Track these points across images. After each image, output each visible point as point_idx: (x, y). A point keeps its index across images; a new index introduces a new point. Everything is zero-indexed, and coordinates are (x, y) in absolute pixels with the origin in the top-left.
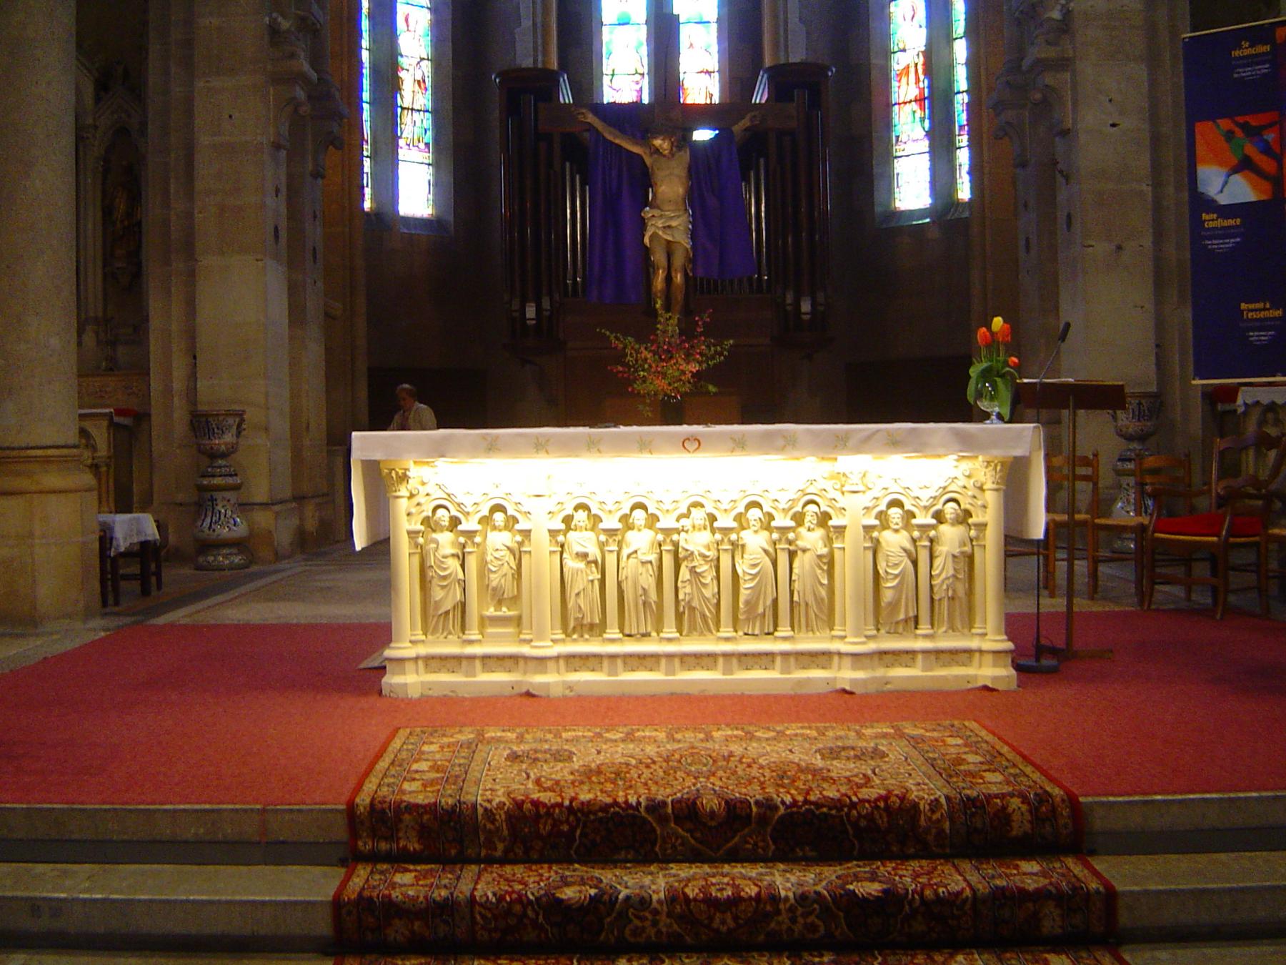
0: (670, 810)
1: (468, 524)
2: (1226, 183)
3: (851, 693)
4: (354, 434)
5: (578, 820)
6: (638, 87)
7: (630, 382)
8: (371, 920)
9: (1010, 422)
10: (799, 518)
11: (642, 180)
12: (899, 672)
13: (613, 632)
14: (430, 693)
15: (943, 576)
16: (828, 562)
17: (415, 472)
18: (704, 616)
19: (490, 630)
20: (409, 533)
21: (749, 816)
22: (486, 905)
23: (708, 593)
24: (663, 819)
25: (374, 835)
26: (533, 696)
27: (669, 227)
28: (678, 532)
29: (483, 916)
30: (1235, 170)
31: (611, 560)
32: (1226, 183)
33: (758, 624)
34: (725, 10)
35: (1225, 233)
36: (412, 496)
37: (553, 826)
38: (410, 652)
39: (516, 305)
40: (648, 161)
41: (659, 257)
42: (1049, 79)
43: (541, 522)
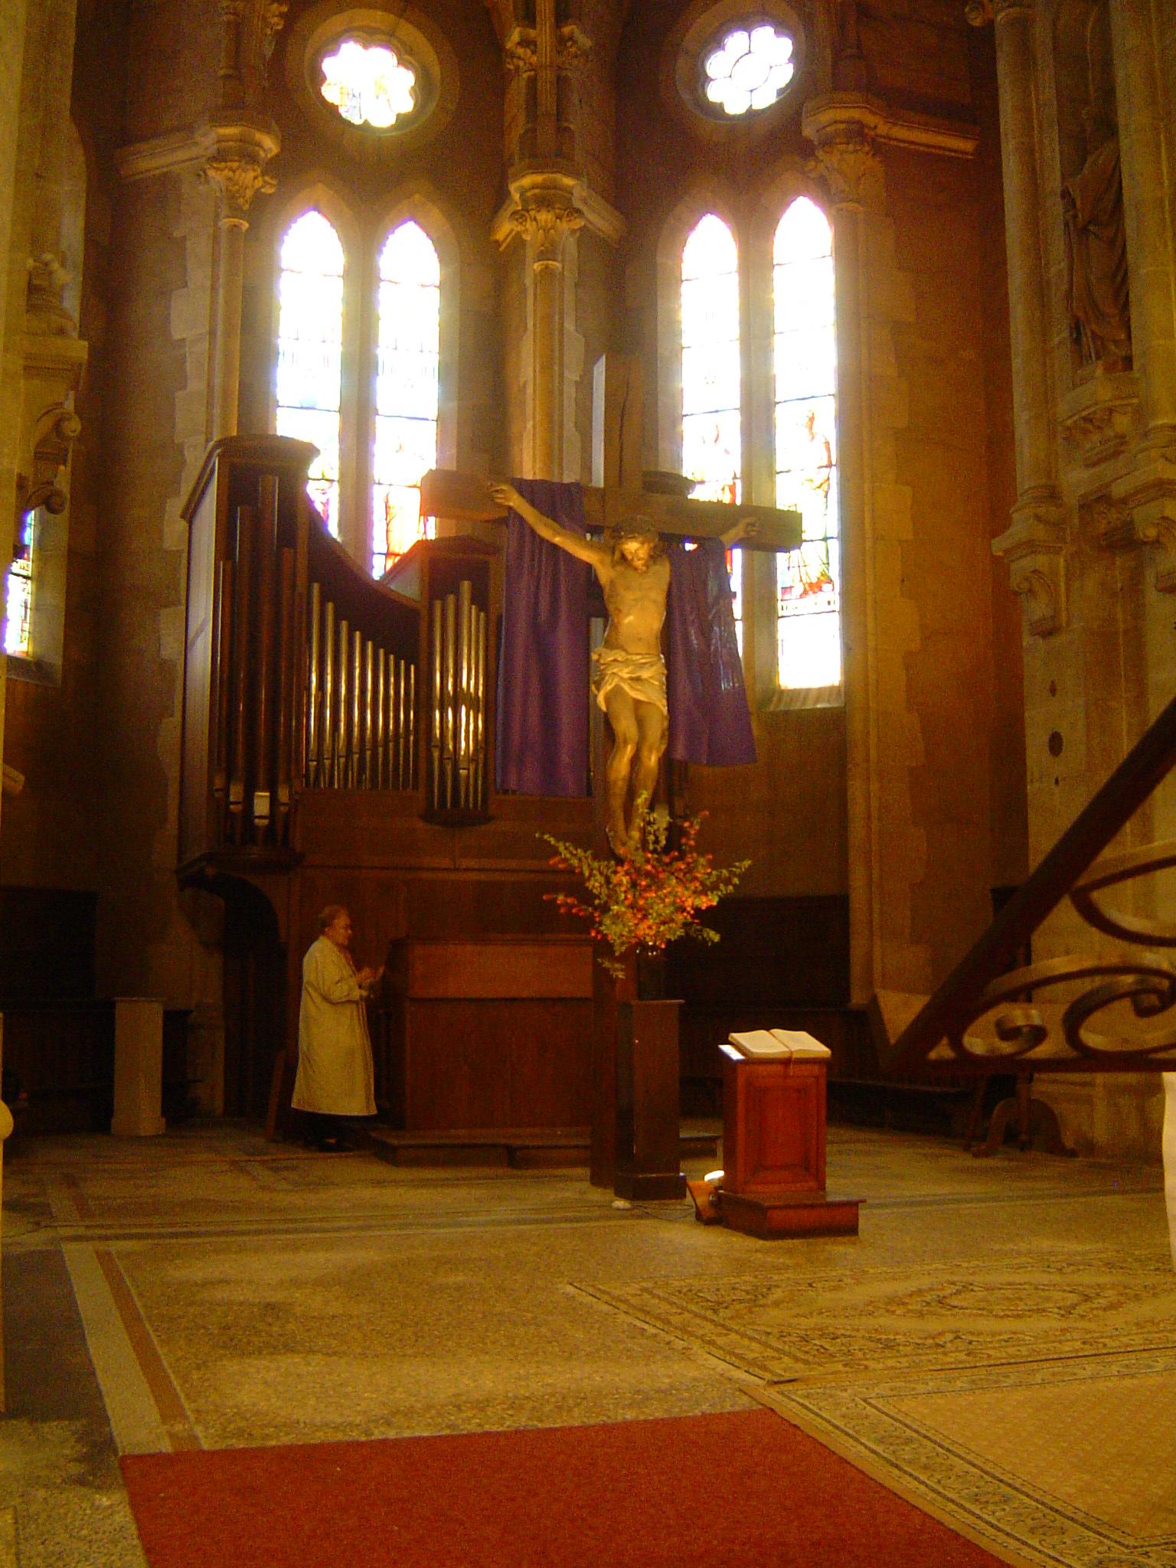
4: (294, 1105)
7: (589, 923)
11: (593, 602)
27: (638, 679)
34: (453, 405)
39: (236, 792)
40: (605, 574)
41: (625, 726)
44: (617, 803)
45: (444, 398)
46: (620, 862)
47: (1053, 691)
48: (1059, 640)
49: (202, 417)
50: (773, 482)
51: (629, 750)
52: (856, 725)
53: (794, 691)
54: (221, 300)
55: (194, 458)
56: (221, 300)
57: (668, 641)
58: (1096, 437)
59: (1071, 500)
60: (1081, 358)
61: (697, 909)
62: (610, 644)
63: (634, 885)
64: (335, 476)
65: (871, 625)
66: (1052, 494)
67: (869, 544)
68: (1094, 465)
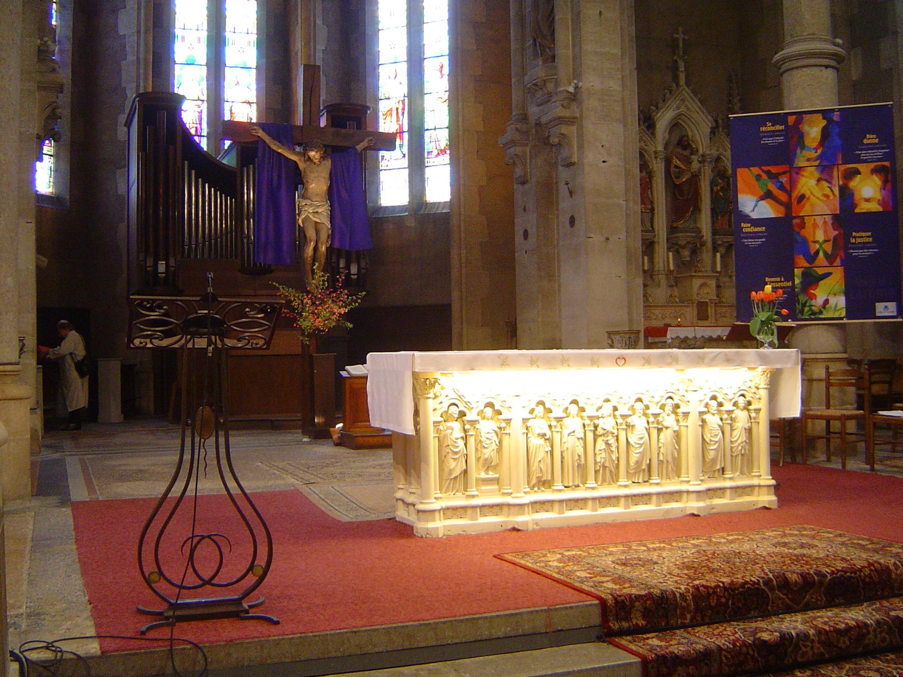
0: (775, 582)
1: (470, 416)
2: (756, 206)
3: (699, 516)
5: (730, 594)
6: (199, 110)
7: (295, 320)
8: (665, 669)
9: (778, 348)
10: (663, 407)
11: (297, 179)
12: (717, 501)
13: (558, 485)
14: (449, 533)
15: (740, 441)
16: (677, 435)
17: (443, 380)
18: (611, 471)
19: (483, 488)
20: (434, 422)
21: (814, 581)
22: (728, 651)
23: (614, 457)
24: (772, 589)
25: (618, 618)
26: (518, 530)
27: (317, 212)
28: (598, 418)
29: (726, 657)
30: (762, 198)
31: (557, 437)
32: (756, 206)
33: (641, 477)
35: (755, 235)
36: (436, 396)
37: (718, 600)
38: (437, 505)
39: (150, 262)
40: (301, 165)
41: (311, 233)
42: (564, 129)
43: (694, 407)
44: (308, 268)
45: (259, 57)
46: (308, 293)
47: (525, 210)
48: (527, 186)
49: (134, 74)
50: (423, 99)
51: (312, 244)
52: (454, 221)
53: (434, 203)
54: (142, 15)
55: (131, 95)
56: (142, 15)
57: (331, 194)
58: (540, 93)
59: (532, 120)
60: (536, 55)
61: (340, 314)
62: (303, 197)
63: (313, 303)
64: (205, 98)
65: (461, 173)
66: (525, 118)
67: (461, 133)
68: (541, 104)
